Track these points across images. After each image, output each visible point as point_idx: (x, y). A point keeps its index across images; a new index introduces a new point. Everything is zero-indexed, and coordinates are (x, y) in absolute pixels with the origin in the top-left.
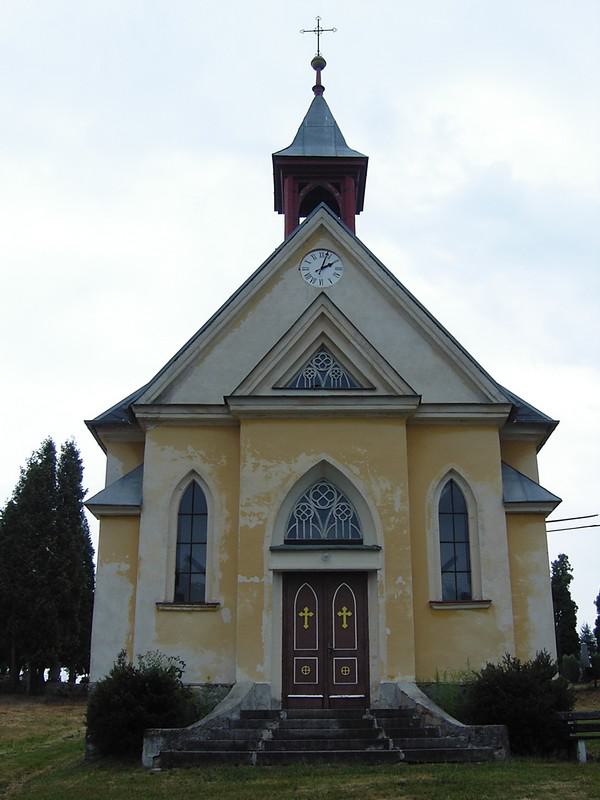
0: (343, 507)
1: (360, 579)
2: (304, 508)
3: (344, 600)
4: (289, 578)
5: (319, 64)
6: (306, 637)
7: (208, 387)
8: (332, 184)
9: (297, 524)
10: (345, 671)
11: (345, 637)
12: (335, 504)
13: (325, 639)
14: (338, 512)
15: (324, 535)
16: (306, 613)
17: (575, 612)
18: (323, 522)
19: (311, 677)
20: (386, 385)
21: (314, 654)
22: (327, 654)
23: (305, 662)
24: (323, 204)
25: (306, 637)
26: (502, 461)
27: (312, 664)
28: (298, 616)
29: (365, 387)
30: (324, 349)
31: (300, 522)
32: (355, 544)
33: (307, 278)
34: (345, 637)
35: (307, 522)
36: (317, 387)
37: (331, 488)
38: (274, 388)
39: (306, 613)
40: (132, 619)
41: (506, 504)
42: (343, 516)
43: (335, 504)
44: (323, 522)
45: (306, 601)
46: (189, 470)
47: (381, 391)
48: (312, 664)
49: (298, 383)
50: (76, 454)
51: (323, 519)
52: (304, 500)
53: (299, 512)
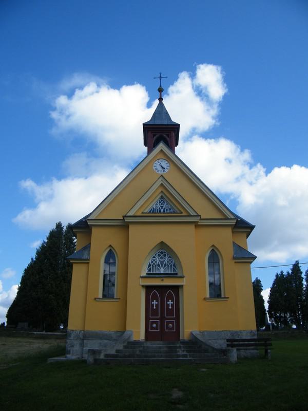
1: (177, 288)
3: (170, 297)
4: (148, 288)
5: (166, 77)
6: (155, 312)
7: (148, 123)
8: (167, 135)
11: (170, 312)
13: (162, 313)
20: (187, 211)
22: (162, 319)
25: (155, 312)
27: (157, 323)
29: (178, 212)
36: (160, 212)
39: (155, 303)
44: (162, 267)
45: (155, 297)
48: (157, 323)
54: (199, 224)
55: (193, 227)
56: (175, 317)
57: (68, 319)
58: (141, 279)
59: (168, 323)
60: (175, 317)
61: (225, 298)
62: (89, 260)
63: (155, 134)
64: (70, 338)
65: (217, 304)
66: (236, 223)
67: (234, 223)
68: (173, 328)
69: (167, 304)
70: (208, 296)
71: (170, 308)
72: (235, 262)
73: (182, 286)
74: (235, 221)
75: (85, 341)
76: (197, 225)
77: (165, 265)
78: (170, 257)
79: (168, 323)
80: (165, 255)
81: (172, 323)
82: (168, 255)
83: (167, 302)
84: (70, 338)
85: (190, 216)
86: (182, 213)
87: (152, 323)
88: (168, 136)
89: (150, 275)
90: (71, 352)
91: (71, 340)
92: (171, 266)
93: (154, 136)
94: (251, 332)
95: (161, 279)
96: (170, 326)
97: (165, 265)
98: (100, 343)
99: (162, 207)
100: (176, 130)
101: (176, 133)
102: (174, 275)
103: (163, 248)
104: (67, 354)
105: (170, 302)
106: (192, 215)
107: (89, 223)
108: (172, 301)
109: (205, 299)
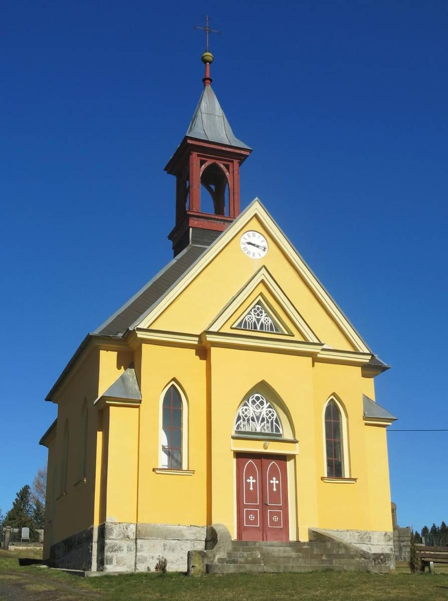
0: (270, 412)
1: (283, 458)
3: (274, 473)
4: (239, 455)
6: (251, 496)
8: (224, 165)
11: (275, 497)
12: (265, 409)
15: (258, 430)
16: (251, 480)
18: (258, 422)
19: (272, 514)
21: (256, 507)
22: (264, 505)
23: (251, 512)
24: (256, 207)
25: (251, 496)
26: (392, 503)
27: (255, 513)
29: (286, 333)
30: (260, 305)
33: (245, 250)
34: (275, 497)
37: (262, 399)
38: (231, 328)
39: (251, 480)
41: (365, 418)
42: (270, 418)
43: (265, 409)
44: (258, 422)
45: (250, 472)
46: (172, 378)
47: (298, 337)
49: (243, 325)
50: (117, 367)
54: (319, 356)
55: (309, 360)
56: (281, 505)
58: (232, 440)
59: (272, 514)
60: (258, 510)
61: (350, 479)
62: (140, 402)
63: (203, 159)
64: (111, 537)
65: (336, 486)
67: (368, 361)
70: (326, 475)
71: (275, 489)
72: (366, 424)
73: (293, 457)
74: (369, 357)
75: (138, 541)
76: (315, 359)
78: (269, 407)
79: (248, 521)
80: (262, 403)
82: (267, 403)
83: (256, 482)
84: (111, 537)
85: (307, 343)
86: (293, 336)
87: (248, 513)
88: (227, 167)
89: (241, 436)
90: (114, 562)
91: (113, 539)
93: (202, 163)
94: (385, 535)
95: (263, 443)
96: (275, 519)
98: (165, 545)
99: (258, 320)
102: (276, 437)
103: (264, 390)
104: (107, 564)
105: (274, 481)
106: (311, 341)
107: (139, 336)
108: (278, 479)
109: (322, 479)
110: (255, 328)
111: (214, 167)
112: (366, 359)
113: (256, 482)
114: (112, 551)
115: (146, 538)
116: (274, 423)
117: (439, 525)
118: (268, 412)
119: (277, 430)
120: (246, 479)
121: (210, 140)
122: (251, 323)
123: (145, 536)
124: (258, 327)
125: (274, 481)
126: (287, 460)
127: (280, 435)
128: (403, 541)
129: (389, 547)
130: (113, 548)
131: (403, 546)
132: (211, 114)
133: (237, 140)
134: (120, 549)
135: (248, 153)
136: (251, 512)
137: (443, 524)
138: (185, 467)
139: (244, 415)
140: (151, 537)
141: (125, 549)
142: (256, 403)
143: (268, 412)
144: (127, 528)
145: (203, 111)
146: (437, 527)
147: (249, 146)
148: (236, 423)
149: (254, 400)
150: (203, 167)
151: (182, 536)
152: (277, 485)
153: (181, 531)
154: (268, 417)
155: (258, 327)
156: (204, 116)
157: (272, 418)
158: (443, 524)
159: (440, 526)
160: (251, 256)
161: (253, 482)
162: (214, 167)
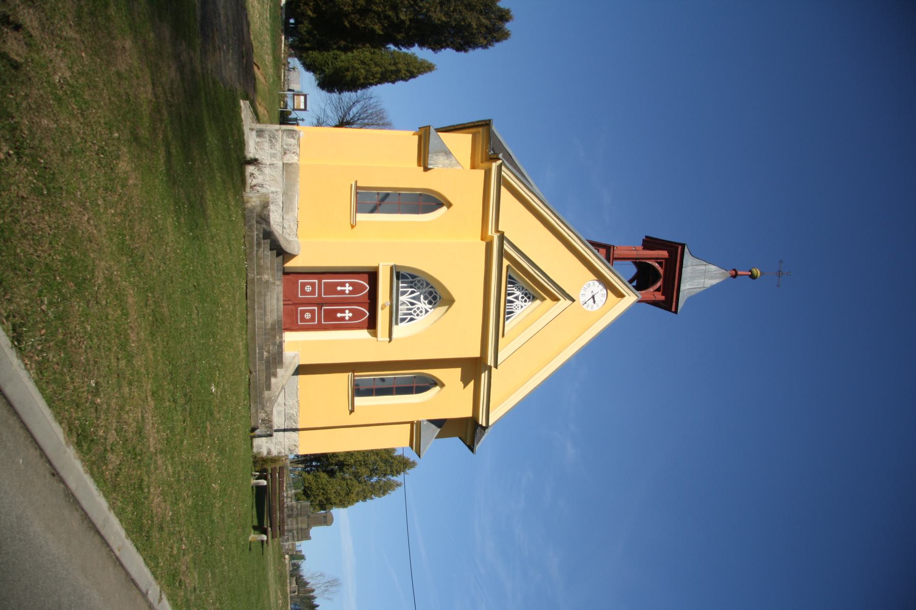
1: (372, 325)
2: (422, 284)
3: (357, 315)
5: (778, 286)
8: (660, 287)
9: (411, 280)
10: (308, 316)
11: (330, 315)
14: (418, 309)
15: (402, 298)
17: (430, 47)
19: (312, 312)
23: (314, 288)
27: (313, 292)
28: (346, 282)
31: (410, 309)
32: (394, 319)
35: (411, 314)
40: (246, 292)
51: (414, 298)
52: (428, 284)
53: (419, 281)
56: (317, 281)
57: (348, 452)
59: (312, 312)
60: (317, 281)
65: (346, 199)
66: (481, 426)
67: (480, 423)
68: (303, 319)
69: (349, 320)
73: (375, 335)
74: (484, 425)
77: (412, 304)
81: (312, 319)
83: (346, 294)
90: (258, 140)
92: (411, 314)
97: (412, 304)
100: (680, 247)
101: (662, 304)
105: (348, 315)
108: (350, 319)
110: (510, 294)
111: (655, 276)
112: (482, 421)
113: (346, 294)
114: (270, 137)
115: (284, 173)
116: (409, 317)
117: (316, 602)
118: (421, 309)
119: (403, 320)
120: (349, 283)
121: (683, 269)
122: (513, 290)
123: (287, 171)
124: (509, 298)
125: (348, 315)
126: (370, 330)
127: (397, 324)
128: (297, 532)
129: (283, 451)
130: (273, 138)
131: (293, 534)
132: (705, 274)
133: (685, 299)
134: (272, 145)
135: (673, 310)
136: (314, 288)
137: (317, 606)
138: (361, 217)
139: (416, 282)
140: (286, 178)
141: (273, 151)
142: (430, 296)
143: (421, 309)
144: (294, 152)
145: (707, 267)
146: (316, 600)
147: (682, 307)
148: (408, 274)
149: (433, 293)
150: (657, 264)
151: (287, 213)
152: (343, 319)
153: (292, 211)
154: (416, 309)
155: (509, 298)
156: (703, 267)
157: (415, 314)
158: (317, 606)
159: (315, 603)
160: (582, 292)
161: (345, 290)
162: (655, 276)
